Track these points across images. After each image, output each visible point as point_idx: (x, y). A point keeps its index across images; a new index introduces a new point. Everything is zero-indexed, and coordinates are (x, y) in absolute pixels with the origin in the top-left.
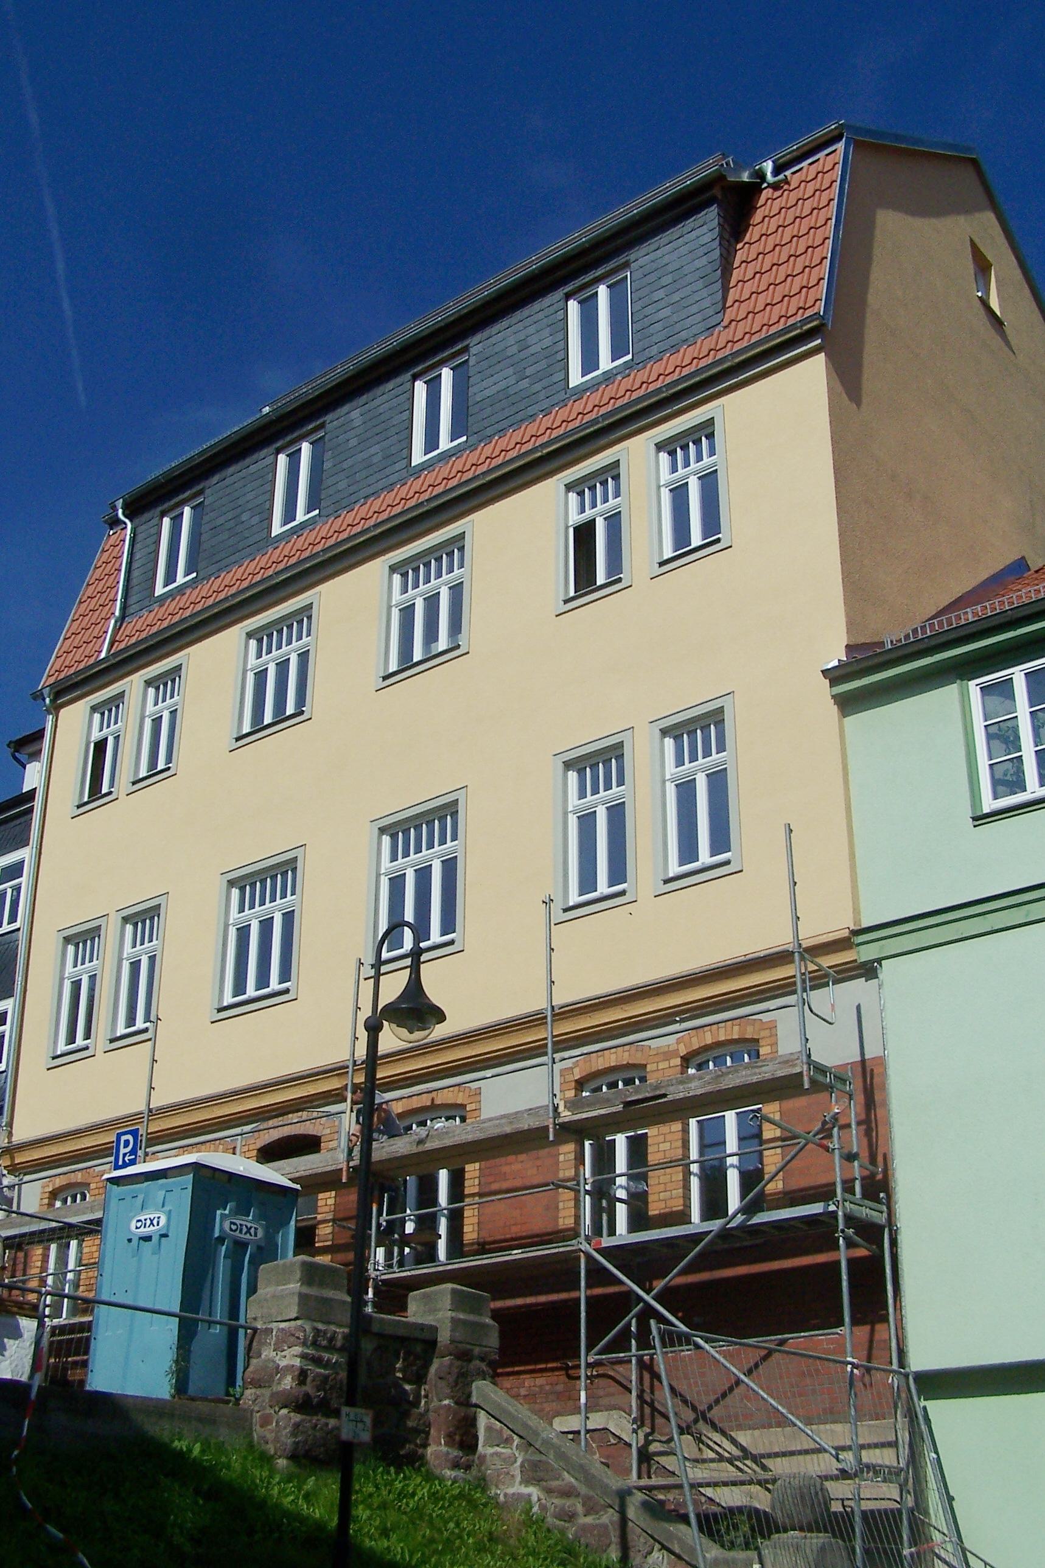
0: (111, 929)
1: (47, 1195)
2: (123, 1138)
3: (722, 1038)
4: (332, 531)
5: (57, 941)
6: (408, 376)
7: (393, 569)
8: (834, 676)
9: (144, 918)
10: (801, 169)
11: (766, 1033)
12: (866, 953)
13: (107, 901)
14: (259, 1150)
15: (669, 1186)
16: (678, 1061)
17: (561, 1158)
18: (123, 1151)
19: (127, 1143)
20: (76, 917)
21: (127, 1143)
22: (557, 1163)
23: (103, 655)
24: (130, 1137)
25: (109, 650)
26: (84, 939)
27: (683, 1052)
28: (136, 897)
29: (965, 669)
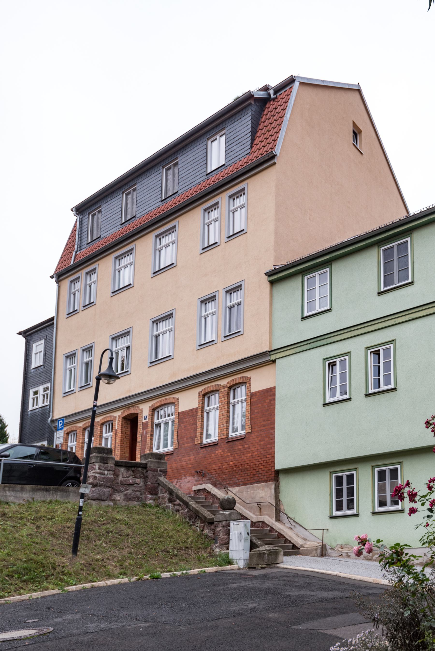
0: (79, 354)
1: (151, 411)
2: (60, 422)
3: (238, 382)
4: (259, 154)
5: (63, 358)
6: (205, 139)
7: (205, 210)
8: (269, 274)
9: (88, 349)
10: (286, 90)
11: (248, 380)
12: (273, 358)
13: (77, 346)
14: (122, 418)
15: (223, 423)
16: (227, 389)
17: (198, 416)
18: (60, 425)
19: (61, 423)
20: (69, 350)
21: (61, 423)
22: (197, 418)
23: (72, 263)
24: (61, 421)
25: (74, 261)
26: (71, 356)
27: (228, 386)
28: (86, 344)
29: (379, 243)
